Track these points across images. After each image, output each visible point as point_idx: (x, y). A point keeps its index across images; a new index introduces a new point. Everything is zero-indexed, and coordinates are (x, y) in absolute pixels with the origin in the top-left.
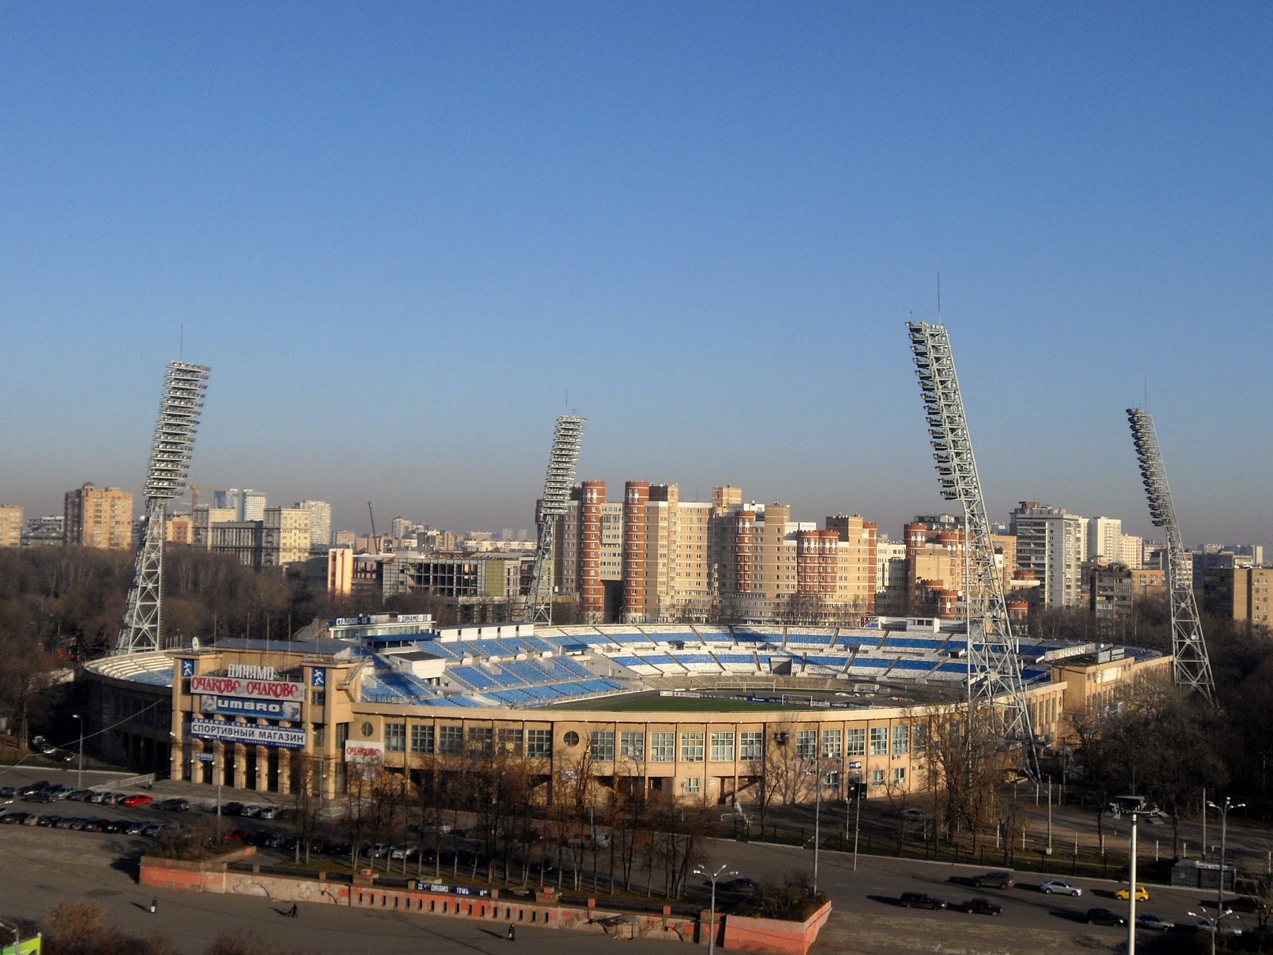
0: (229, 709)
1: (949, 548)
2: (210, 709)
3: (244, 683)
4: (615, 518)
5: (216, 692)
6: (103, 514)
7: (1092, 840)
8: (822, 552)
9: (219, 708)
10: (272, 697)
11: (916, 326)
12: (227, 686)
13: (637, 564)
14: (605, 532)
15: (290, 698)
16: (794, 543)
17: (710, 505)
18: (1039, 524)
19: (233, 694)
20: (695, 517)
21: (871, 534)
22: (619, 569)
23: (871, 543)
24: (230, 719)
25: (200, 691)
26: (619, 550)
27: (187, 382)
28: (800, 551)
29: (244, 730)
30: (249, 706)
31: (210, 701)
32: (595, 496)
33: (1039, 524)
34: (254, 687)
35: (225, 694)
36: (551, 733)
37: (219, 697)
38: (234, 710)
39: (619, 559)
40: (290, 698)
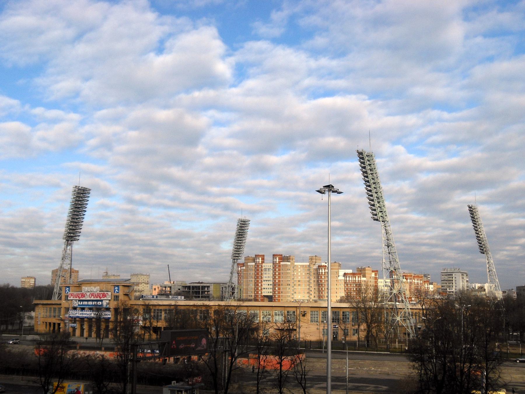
0: (83, 305)
1: (409, 281)
2: (75, 306)
3: (88, 294)
4: (269, 269)
5: (78, 299)
9: (79, 305)
10: (99, 299)
11: (360, 151)
12: (82, 296)
15: (105, 298)
17: (308, 264)
18: (450, 275)
19: (84, 299)
21: (376, 275)
22: (271, 290)
23: (376, 278)
24: (83, 309)
25: (72, 298)
26: (271, 283)
27: (81, 197)
29: (88, 313)
30: (90, 303)
31: (75, 303)
33: (450, 275)
34: (92, 295)
35: (81, 299)
36: (208, 311)
37: (79, 300)
38: (84, 305)
39: (271, 287)
40: (105, 298)
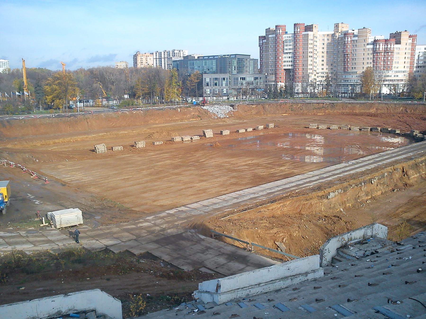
6: (143, 62)
7: (159, 215)
8: (386, 51)
13: (300, 62)
14: (285, 47)
16: (371, 46)
17: (333, 33)
20: (326, 39)
28: (375, 51)
32: (281, 31)
